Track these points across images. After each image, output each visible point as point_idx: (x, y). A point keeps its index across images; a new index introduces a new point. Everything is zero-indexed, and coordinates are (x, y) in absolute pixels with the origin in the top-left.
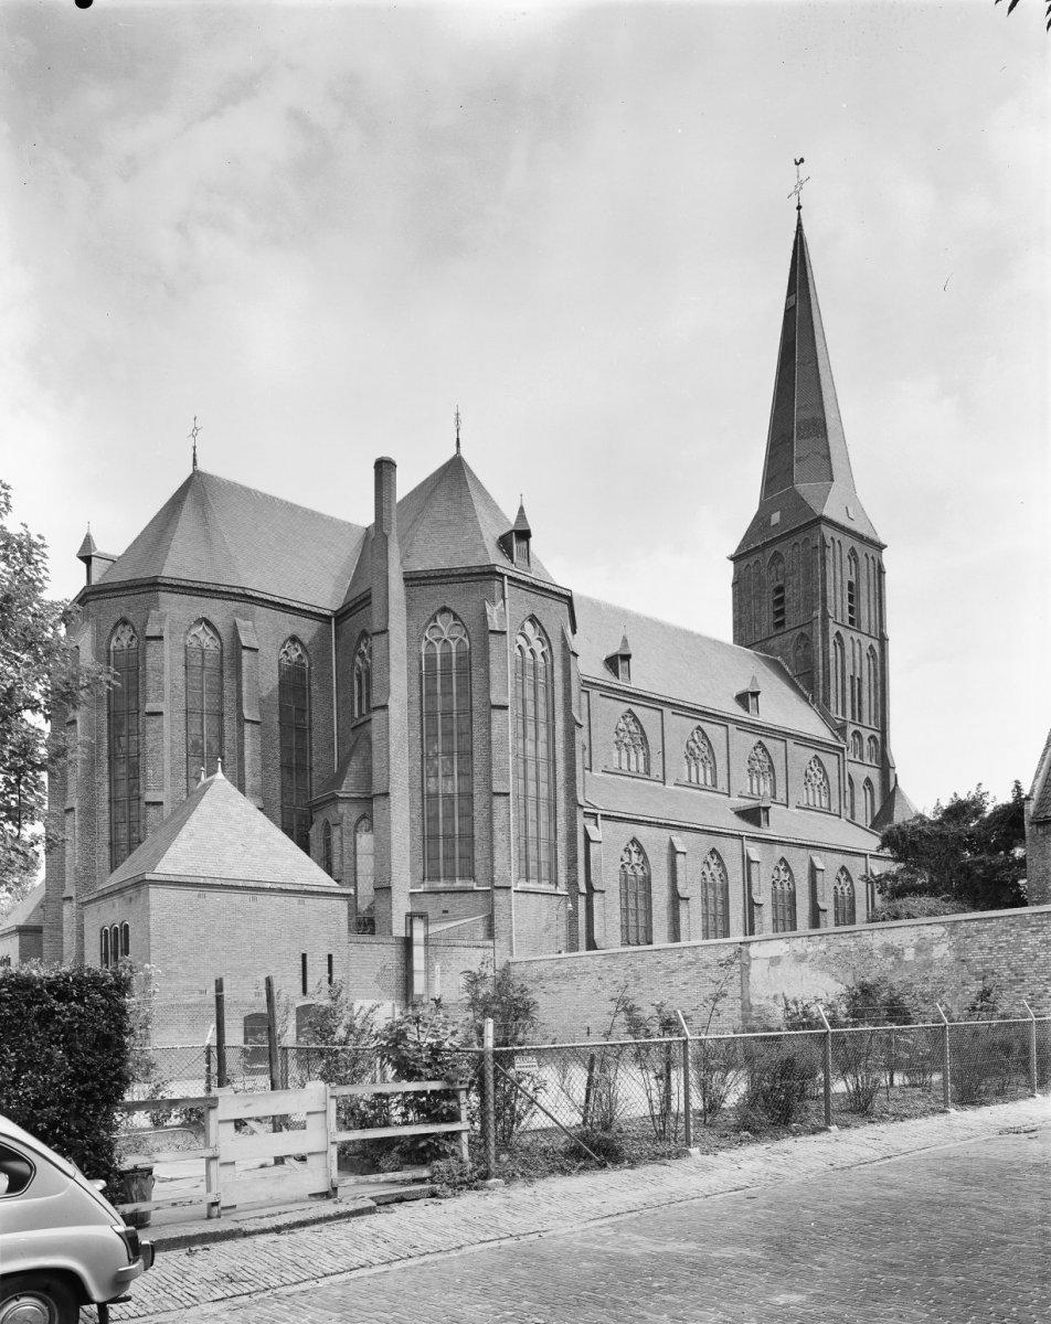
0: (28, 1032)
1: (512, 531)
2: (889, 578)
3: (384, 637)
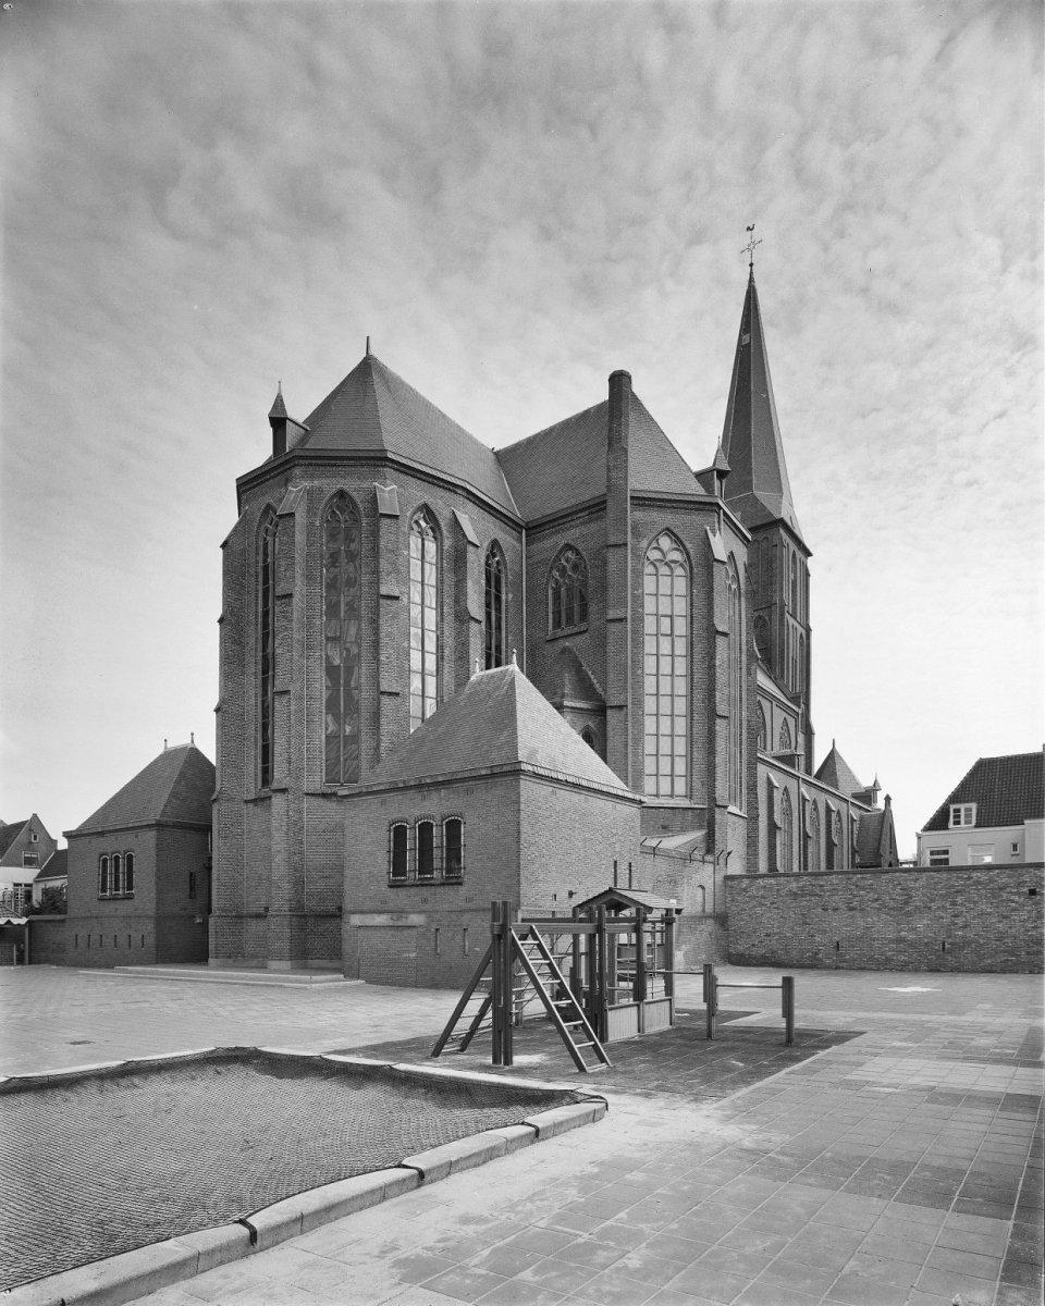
0: (816, 954)
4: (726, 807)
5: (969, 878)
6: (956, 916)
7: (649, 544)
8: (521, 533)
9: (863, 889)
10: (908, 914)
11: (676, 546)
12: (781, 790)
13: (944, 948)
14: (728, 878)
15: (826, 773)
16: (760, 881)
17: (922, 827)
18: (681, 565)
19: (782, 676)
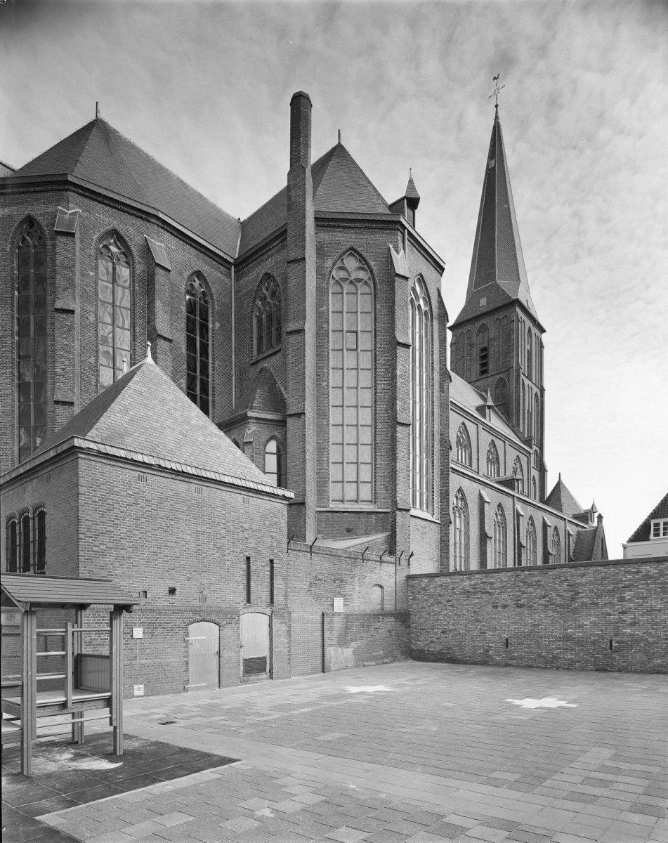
0: (487, 651)
1: (402, 199)
2: (545, 351)
3: (299, 266)
4: (408, 510)
5: (638, 572)
6: (624, 613)
7: (334, 264)
8: (230, 269)
9: (530, 585)
10: (575, 611)
11: (360, 265)
12: (553, 528)
13: (611, 645)
14: (410, 577)
15: (553, 500)
16: (437, 579)
17: (627, 540)
18: (366, 283)
19: (518, 425)
